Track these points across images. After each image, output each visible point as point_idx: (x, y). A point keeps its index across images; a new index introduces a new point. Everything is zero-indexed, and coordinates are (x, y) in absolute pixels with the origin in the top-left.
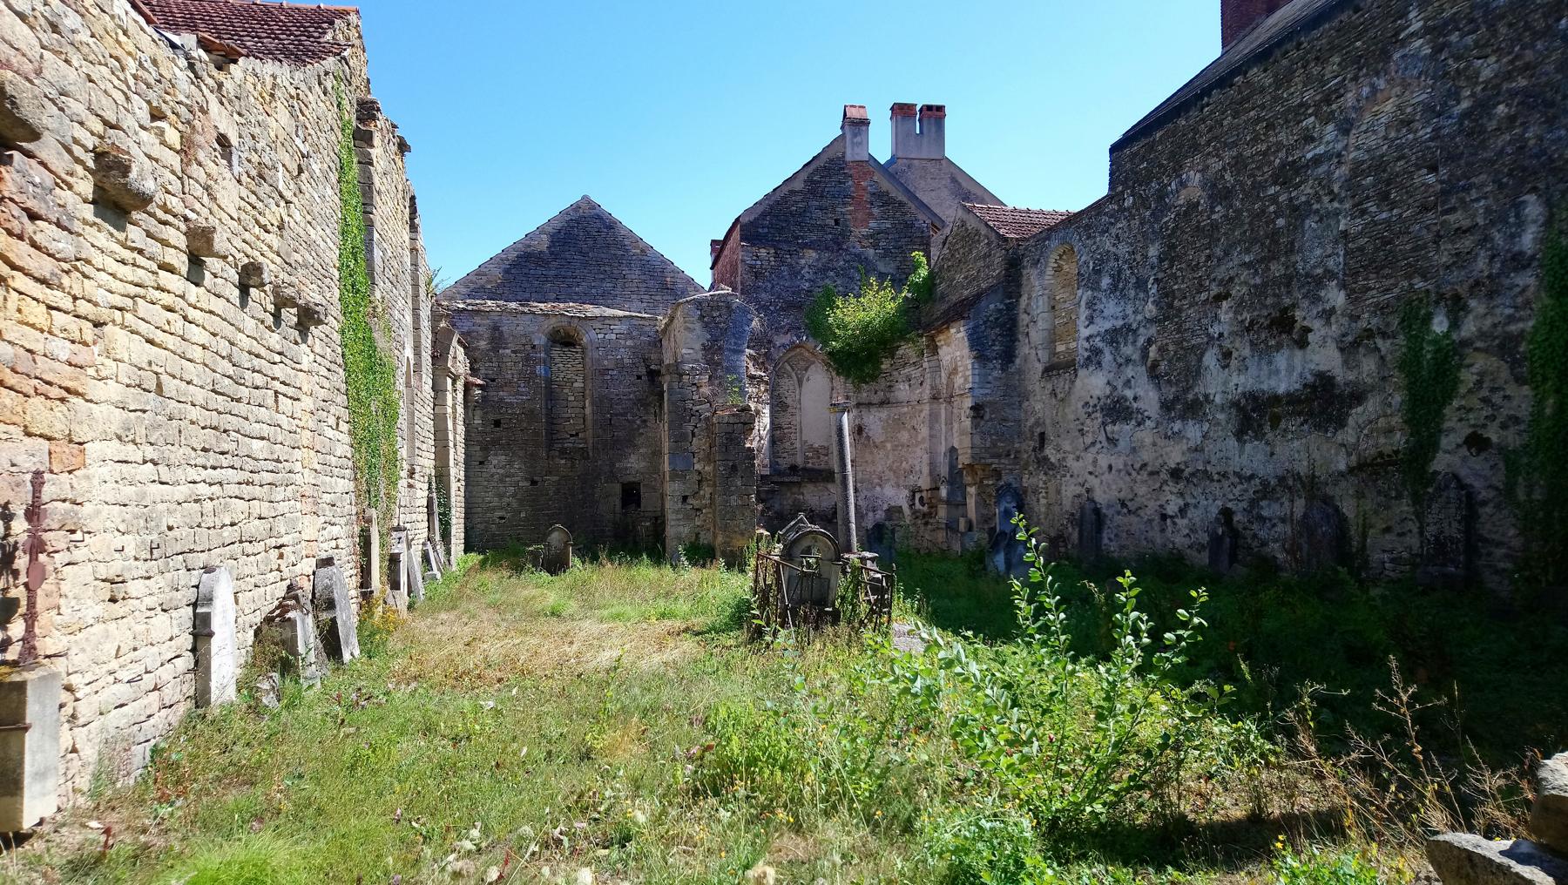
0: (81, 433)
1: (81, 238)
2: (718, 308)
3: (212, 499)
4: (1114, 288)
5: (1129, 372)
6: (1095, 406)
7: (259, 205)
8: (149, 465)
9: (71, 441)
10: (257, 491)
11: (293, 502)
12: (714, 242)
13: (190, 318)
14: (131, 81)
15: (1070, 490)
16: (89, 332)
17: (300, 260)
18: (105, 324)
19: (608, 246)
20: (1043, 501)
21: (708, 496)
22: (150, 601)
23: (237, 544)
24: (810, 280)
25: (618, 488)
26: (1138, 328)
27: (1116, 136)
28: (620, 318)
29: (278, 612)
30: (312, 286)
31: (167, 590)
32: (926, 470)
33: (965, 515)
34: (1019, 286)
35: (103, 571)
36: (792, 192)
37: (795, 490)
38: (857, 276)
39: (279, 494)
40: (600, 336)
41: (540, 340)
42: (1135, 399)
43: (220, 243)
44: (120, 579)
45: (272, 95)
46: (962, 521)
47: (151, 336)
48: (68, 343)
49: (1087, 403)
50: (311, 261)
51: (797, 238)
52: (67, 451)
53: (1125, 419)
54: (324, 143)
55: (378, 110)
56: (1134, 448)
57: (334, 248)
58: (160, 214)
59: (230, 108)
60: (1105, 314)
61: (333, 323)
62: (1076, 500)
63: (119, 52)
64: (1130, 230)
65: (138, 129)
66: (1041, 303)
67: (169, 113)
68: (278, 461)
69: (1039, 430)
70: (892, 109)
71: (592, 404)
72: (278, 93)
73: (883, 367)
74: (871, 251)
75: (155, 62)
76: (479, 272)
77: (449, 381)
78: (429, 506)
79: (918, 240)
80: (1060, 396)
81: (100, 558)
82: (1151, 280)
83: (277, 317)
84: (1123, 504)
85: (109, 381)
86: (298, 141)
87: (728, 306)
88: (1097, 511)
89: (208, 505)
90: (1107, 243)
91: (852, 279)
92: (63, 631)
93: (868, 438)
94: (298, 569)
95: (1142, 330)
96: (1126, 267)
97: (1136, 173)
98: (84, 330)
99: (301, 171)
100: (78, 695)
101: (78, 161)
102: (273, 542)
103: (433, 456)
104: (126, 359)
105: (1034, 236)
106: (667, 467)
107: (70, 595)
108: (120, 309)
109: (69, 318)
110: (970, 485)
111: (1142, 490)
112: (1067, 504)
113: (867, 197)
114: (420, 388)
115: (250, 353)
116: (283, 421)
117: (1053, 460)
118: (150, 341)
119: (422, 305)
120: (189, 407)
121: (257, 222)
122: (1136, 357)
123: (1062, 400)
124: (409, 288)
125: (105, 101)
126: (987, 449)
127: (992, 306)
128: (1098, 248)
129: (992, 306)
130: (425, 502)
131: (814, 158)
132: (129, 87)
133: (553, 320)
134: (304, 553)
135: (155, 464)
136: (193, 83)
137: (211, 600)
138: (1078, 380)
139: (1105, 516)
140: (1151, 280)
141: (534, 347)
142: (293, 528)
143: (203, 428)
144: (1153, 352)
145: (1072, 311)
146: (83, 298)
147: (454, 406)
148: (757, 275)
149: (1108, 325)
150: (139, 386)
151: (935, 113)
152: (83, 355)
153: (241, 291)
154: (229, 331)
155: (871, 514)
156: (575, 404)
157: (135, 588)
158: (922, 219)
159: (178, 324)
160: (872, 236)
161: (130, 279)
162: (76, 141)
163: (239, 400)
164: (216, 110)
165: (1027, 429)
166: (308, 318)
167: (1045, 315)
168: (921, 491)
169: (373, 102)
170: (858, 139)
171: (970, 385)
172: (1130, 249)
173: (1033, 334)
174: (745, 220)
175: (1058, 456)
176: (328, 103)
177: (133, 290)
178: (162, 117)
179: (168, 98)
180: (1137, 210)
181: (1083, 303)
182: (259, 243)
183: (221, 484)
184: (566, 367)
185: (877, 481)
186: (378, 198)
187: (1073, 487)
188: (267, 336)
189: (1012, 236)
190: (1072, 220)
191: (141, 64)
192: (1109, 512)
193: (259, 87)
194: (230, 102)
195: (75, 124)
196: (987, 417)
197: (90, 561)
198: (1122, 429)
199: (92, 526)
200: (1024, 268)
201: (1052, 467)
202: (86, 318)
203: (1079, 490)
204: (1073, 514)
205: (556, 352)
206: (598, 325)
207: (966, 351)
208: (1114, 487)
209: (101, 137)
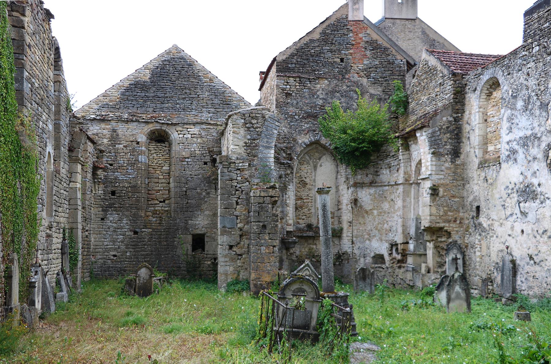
2: (256, 118)
4: (526, 109)
5: (535, 166)
6: (513, 189)
12: (262, 73)
15: (496, 246)
20: (478, 254)
21: (246, 246)
24: (323, 99)
25: (190, 238)
32: (400, 230)
33: (426, 262)
34: (463, 105)
36: (312, 41)
37: (310, 241)
41: (142, 138)
42: (539, 185)
46: (423, 265)
49: (508, 187)
56: (539, 219)
60: (520, 126)
69: (476, 204)
71: (175, 181)
73: (372, 158)
79: (397, 73)
80: (490, 181)
84: (531, 258)
88: (513, 262)
91: (351, 98)
93: (361, 207)
96: (533, 94)
97: (541, 30)
110: (429, 241)
112: (495, 258)
113: (362, 44)
117: (485, 225)
122: (540, 156)
123: (491, 184)
126: (440, 217)
127: (444, 119)
128: (515, 81)
129: (444, 119)
130: (60, 246)
131: (327, 19)
138: (501, 171)
139: (519, 265)
145: (498, 123)
148: (288, 95)
149: (521, 134)
155: (362, 260)
156: (164, 181)
158: (400, 60)
165: (468, 203)
168: (397, 245)
170: (357, 6)
172: (537, 82)
174: (279, 59)
175: (489, 222)
180: (542, 56)
186: (28, 50)
187: (498, 245)
198: (530, 206)
201: (484, 230)
203: (503, 247)
204: (497, 263)
205: (153, 146)
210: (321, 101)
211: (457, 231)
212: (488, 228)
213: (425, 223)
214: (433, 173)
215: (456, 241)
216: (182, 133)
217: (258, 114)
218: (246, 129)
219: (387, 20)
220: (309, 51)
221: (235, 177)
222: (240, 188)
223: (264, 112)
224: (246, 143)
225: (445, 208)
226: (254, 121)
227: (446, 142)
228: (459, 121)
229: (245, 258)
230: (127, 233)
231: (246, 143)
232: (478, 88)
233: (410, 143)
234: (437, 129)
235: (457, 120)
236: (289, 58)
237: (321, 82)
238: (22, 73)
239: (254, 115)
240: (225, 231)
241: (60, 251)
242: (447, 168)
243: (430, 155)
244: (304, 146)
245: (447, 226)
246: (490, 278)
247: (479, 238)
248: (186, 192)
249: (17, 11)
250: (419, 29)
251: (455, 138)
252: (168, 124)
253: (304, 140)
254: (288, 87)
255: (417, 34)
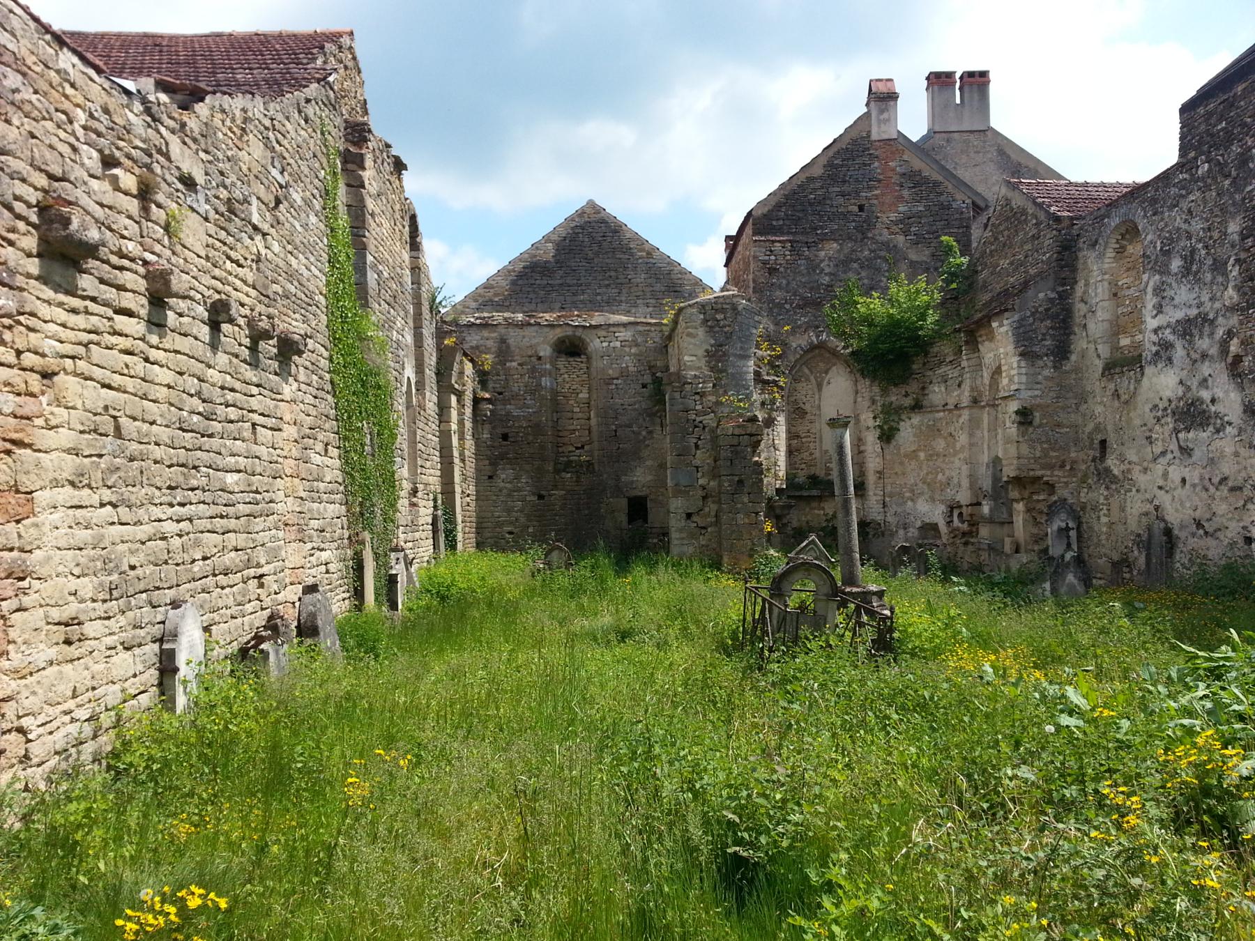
0: (27, 483)
1: (25, 294)
2: (723, 311)
3: (180, 536)
4: (1186, 271)
5: (1206, 369)
6: (1165, 409)
7: (230, 240)
8: (109, 508)
9: (17, 492)
10: (232, 523)
11: (274, 531)
12: (728, 238)
13: (152, 359)
14: (80, 132)
15: (1136, 507)
16: (35, 382)
17: (280, 291)
18: (55, 374)
19: (614, 250)
20: (1104, 520)
21: (713, 513)
22: (110, 641)
23: (211, 578)
24: (830, 274)
25: (624, 503)
26: (1215, 318)
27: (1190, 92)
28: (625, 325)
29: (253, 643)
30: (294, 316)
31: (129, 628)
32: (965, 483)
34: (1074, 270)
35: (55, 614)
36: (811, 179)
37: (814, 504)
38: (885, 266)
39: (259, 523)
40: (605, 344)
41: (546, 351)
42: (1213, 401)
43: (179, 282)
44: (76, 621)
45: (243, 129)
46: (1008, 540)
47: (107, 381)
48: (11, 396)
49: (1156, 406)
50: (293, 290)
51: (816, 229)
52: (13, 502)
53: (1201, 425)
54: (306, 171)
55: (370, 131)
56: (1212, 459)
57: (320, 275)
58: (114, 259)
59: (194, 147)
60: (1176, 302)
61: (317, 352)
62: (1144, 519)
63: (66, 105)
64: (1205, 203)
65: (86, 178)
66: (1100, 290)
67: (123, 160)
68: (257, 492)
69: (1099, 437)
70: (928, 78)
71: (597, 415)
72: (250, 127)
73: (915, 367)
74: (901, 238)
75: (106, 111)
76: (487, 286)
77: (454, 398)
78: (434, 523)
80: (1124, 397)
81: (52, 602)
82: (1232, 261)
83: (253, 349)
84: (1199, 525)
85: (60, 430)
86: (275, 173)
87: (734, 308)
88: (1168, 532)
89: (176, 542)
90: (1177, 219)
91: (878, 270)
92: (12, 675)
94: (280, 597)
95: (1220, 319)
97: (1212, 135)
98: (30, 382)
99: (278, 202)
100: (30, 737)
101: (19, 217)
102: (252, 572)
103: (439, 473)
104: (79, 406)
105: (1091, 213)
106: (670, 483)
107: (19, 640)
108: (73, 358)
109: (15, 371)
110: (1017, 501)
111: (1221, 508)
112: (1133, 525)
113: (895, 179)
114: (422, 407)
115: (222, 388)
116: (263, 451)
117: (1116, 472)
118: (104, 386)
119: (426, 323)
120: (152, 447)
121: (229, 258)
122: (1214, 351)
123: (1127, 402)
124: (411, 308)
125: (48, 154)
126: (1036, 459)
127: (1041, 295)
128: (1166, 225)
129: (1041, 295)
131: (835, 141)
132: (78, 139)
133: (558, 330)
134: (288, 580)
135: (115, 506)
136: (149, 126)
137: (176, 636)
139: (1178, 538)
140: (1232, 261)
141: (540, 358)
142: (274, 556)
143: (169, 467)
144: (1234, 347)
146: (29, 350)
147: (461, 423)
148: (772, 271)
149: (1179, 315)
150: (95, 431)
151: (977, 81)
152: (29, 406)
153: (212, 328)
154: (198, 367)
155: (901, 532)
156: (580, 415)
157: (90, 629)
158: (961, 200)
159: (139, 366)
160: (901, 221)
161: (82, 327)
162: (17, 198)
163: (211, 436)
164: (178, 151)
166: (288, 349)
167: (1106, 304)
168: (960, 507)
169: (365, 124)
170: (885, 115)
171: (1015, 387)
172: (1206, 225)
173: (1091, 326)
176: (310, 130)
177: (85, 337)
178: (115, 163)
179: (122, 144)
180: (1215, 179)
181: (1150, 290)
182: (230, 278)
183: (190, 520)
184: (570, 376)
185: (907, 495)
186: (371, 221)
188: (242, 370)
189: (1066, 214)
190: (1136, 192)
191: (91, 116)
192: (1182, 535)
193: (228, 123)
194: (195, 140)
195: (16, 182)
196: (1037, 421)
197: (41, 606)
199: (43, 572)
200: (1080, 249)
201: (1115, 479)
202: (32, 370)
204: (1139, 535)
205: (562, 362)
206: (602, 333)
207: (1011, 348)
208: (1188, 505)
209: (45, 191)
210: (827, 278)
211: (1065, 483)
212: (1121, 477)
213: (1009, 471)
214: (1023, 387)
215: (1065, 500)
216: (607, 339)
217: (726, 303)
218: (707, 329)
219: (937, 136)
220: (806, 196)
221: (692, 406)
222: (701, 422)
223: (735, 300)
224: (707, 351)
225: (1045, 446)
226: (719, 317)
227: (1044, 335)
228: (1067, 298)
229: (711, 532)
230: (528, 499)
231: (707, 351)
232: (1101, 241)
233: (980, 339)
234: (1028, 314)
235: (1064, 296)
236: (772, 211)
237: (827, 246)
238: (365, 257)
239: (720, 306)
240: (680, 492)
241: (430, 527)
242: (1046, 378)
243: (1017, 358)
244: (801, 352)
245: (1047, 475)
246: (1126, 560)
247: (1105, 493)
248: (616, 431)
249: (353, 163)
250: (993, 146)
251: (1060, 328)
252: (584, 327)
253: (800, 342)
254: (773, 257)
255: (990, 156)
